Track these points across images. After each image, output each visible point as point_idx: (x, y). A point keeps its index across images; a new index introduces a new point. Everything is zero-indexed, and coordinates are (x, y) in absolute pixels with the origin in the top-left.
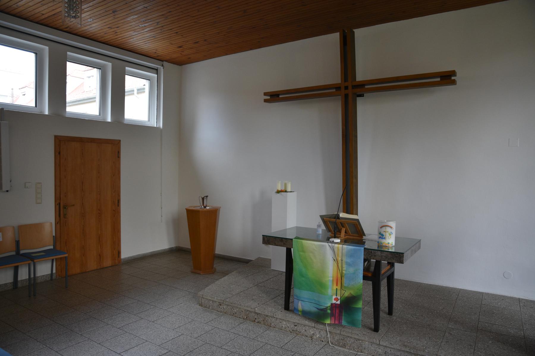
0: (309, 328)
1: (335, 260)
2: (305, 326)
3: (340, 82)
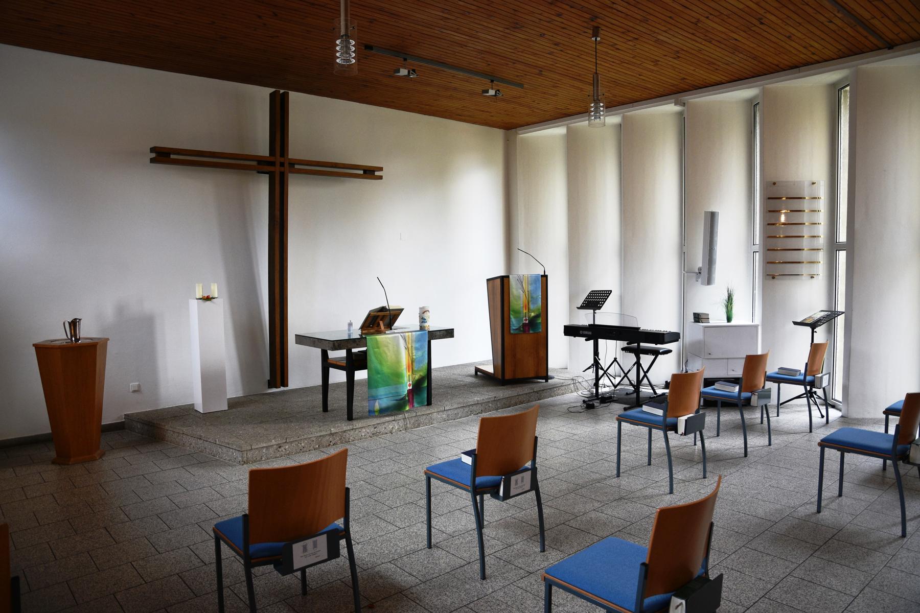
0: (392, 424)
1: (407, 348)
2: (384, 423)
3: (290, 157)
